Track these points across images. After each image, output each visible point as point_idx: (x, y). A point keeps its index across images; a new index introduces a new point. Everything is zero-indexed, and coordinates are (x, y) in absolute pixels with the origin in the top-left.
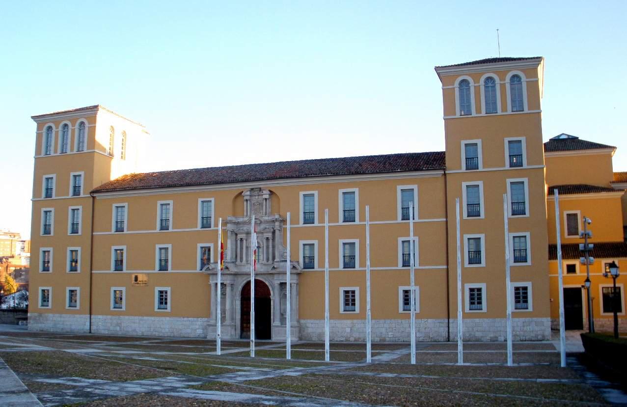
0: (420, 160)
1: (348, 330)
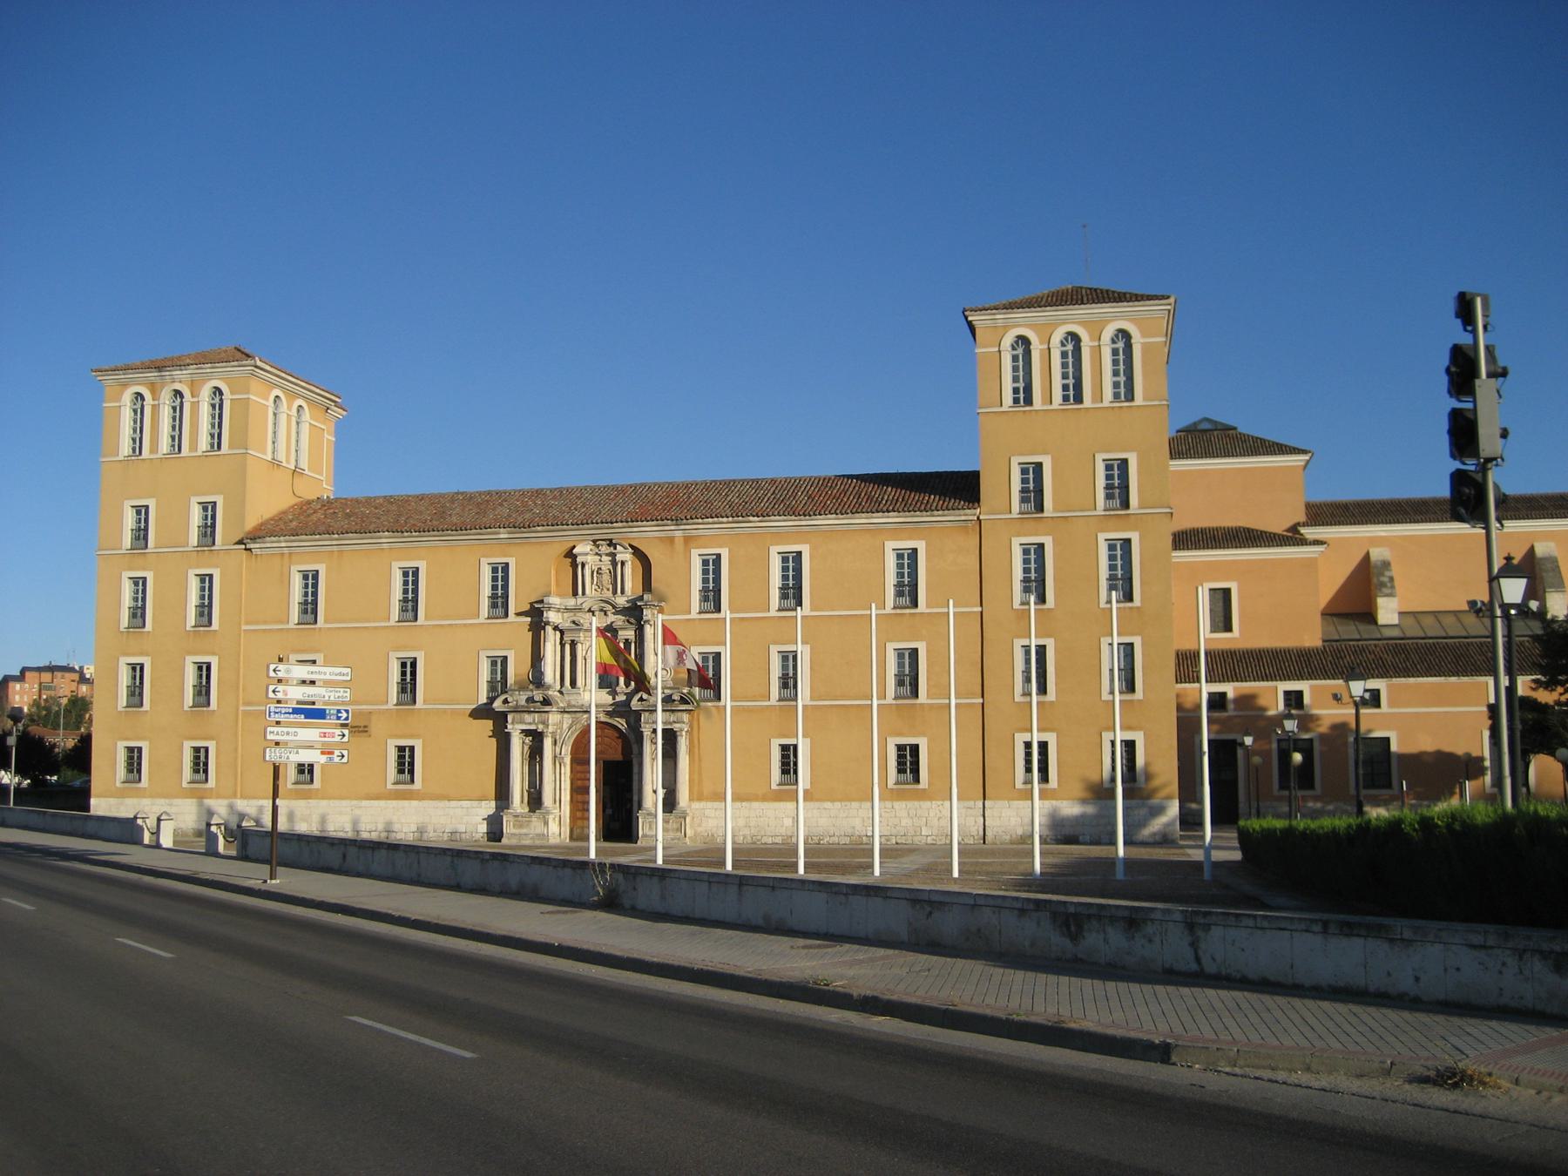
0: (736, 501)
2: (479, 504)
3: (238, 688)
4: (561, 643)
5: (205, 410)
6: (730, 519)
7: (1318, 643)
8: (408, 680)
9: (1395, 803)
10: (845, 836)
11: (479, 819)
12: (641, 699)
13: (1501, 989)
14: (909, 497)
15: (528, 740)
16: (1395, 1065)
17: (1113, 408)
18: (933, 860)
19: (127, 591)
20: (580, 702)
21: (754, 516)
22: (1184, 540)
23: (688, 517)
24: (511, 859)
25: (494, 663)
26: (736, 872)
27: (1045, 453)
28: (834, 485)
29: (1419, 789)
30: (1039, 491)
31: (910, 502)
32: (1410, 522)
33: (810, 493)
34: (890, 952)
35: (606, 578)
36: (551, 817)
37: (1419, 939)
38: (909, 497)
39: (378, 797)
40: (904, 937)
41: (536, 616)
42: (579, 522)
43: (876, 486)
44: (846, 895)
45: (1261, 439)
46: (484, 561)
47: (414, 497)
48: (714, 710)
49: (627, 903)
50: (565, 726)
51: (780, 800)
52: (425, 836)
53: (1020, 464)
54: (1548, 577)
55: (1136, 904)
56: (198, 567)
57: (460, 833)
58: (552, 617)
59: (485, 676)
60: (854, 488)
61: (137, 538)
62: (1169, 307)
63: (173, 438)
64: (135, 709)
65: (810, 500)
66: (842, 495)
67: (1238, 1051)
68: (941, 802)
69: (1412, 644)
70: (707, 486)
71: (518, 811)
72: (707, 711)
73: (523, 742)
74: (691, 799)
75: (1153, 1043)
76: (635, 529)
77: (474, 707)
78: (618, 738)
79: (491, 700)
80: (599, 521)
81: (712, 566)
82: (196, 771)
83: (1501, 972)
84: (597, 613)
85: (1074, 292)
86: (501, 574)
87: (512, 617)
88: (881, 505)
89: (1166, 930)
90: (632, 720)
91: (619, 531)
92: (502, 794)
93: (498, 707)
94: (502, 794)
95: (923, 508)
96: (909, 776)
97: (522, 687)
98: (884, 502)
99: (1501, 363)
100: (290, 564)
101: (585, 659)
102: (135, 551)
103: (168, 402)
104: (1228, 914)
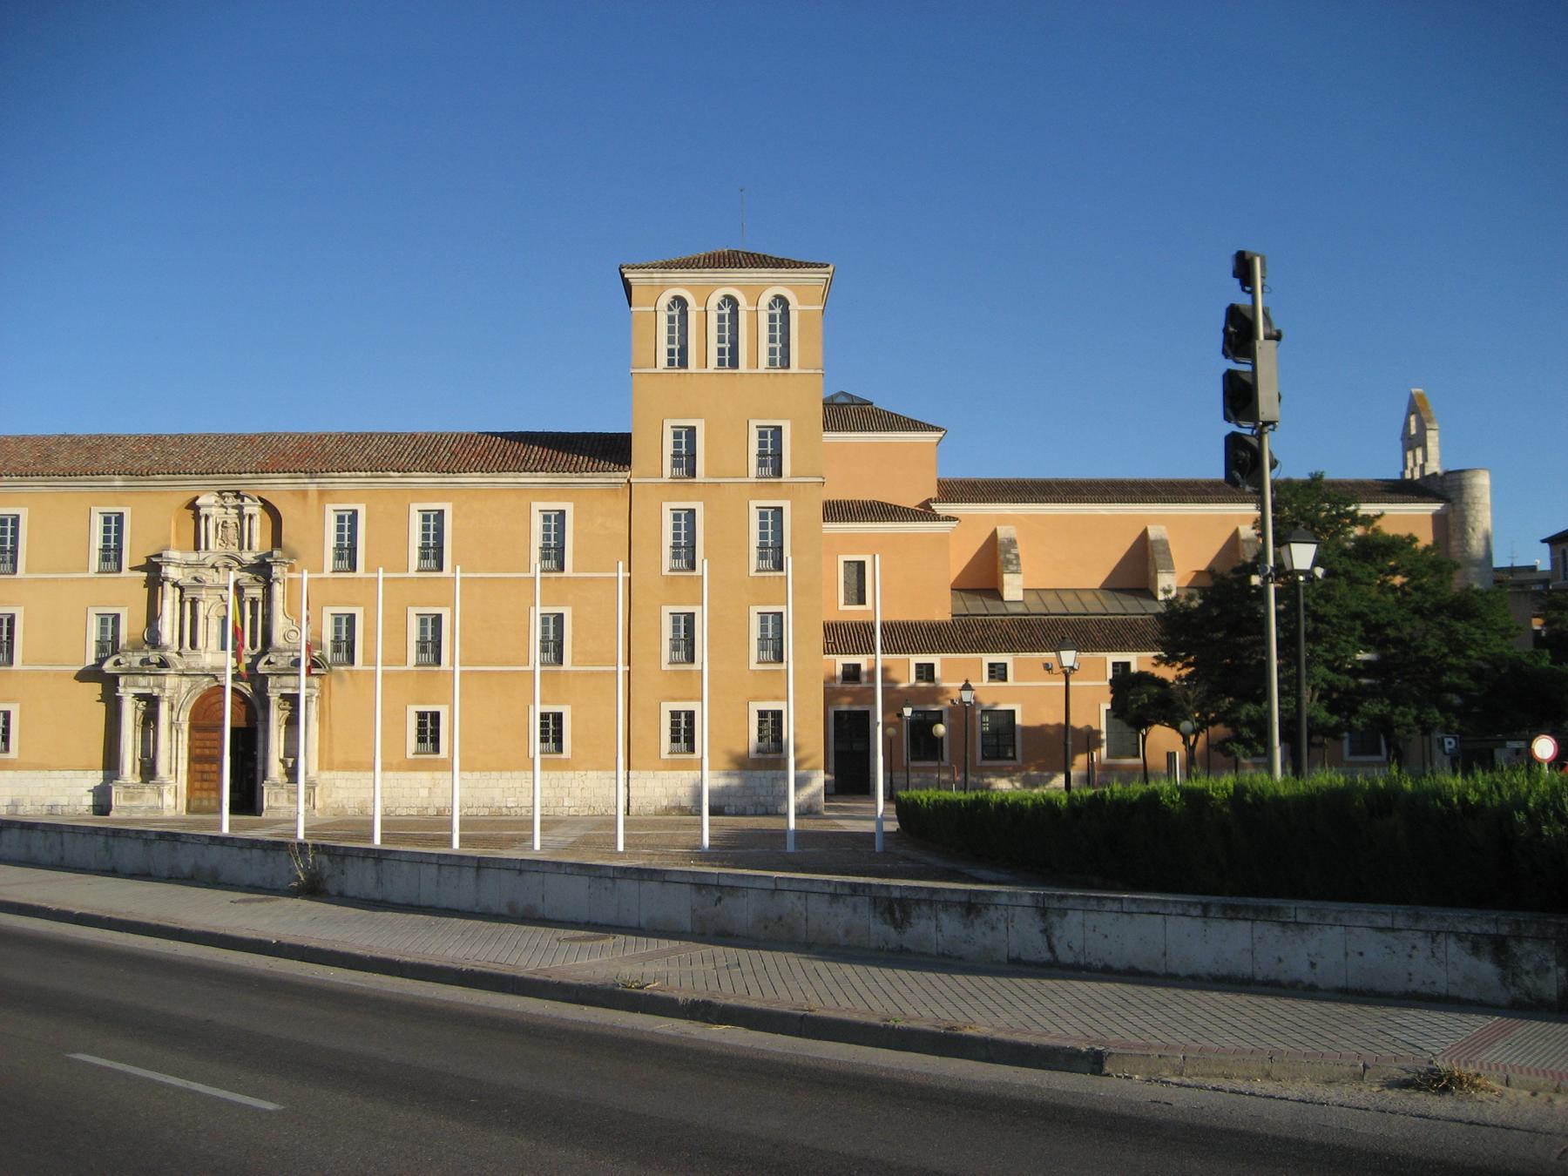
0: (374, 455)
1: (424, 793)
2: (89, 449)
4: (180, 601)
6: (369, 473)
7: (948, 618)
9: (1018, 774)
10: (483, 807)
11: (85, 790)
12: (269, 662)
13: (1410, 974)
14: (557, 456)
15: (142, 705)
16: (1369, 1068)
17: (768, 374)
18: (583, 833)
21: (394, 471)
22: (836, 511)
23: (324, 470)
24: (183, 840)
25: (104, 621)
26: (234, 835)
27: (698, 417)
28: (477, 442)
29: (1041, 761)
30: (692, 456)
31: (558, 462)
32: (1036, 502)
33: (453, 449)
34: (676, 944)
35: (232, 532)
36: (166, 788)
37: (1316, 922)
38: (557, 456)
40: (687, 925)
41: (153, 571)
42: (204, 471)
43: (522, 445)
44: (614, 879)
45: (896, 415)
46: (96, 511)
47: (13, 437)
48: (346, 674)
49: (332, 887)
50: (184, 690)
51: (416, 770)
52: (21, 811)
53: (672, 427)
54: (1159, 559)
55: (862, 880)
57: (62, 806)
58: (171, 572)
59: (94, 634)
60: (499, 446)
62: (827, 276)
65: (454, 457)
66: (487, 453)
67: (1184, 1058)
68: (585, 772)
69: (1036, 619)
70: (343, 438)
71: (129, 782)
72: (340, 675)
73: (136, 707)
74: (321, 768)
75: (1079, 1051)
76: (265, 481)
77: (81, 668)
78: (241, 703)
79: (101, 661)
80: (226, 471)
81: (348, 523)
83: (1410, 956)
84: (221, 570)
85: (731, 256)
86: (113, 525)
87: (125, 571)
88: (529, 464)
89: (1013, 915)
90: (258, 685)
91: (247, 482)
92: (111, 763)
94: (111, 763)
95: (572, 468)
96: (429, 745)
97: (136, 648)
98: (531, 461)
99: (1276, 326)
101: (207, 618)
104: (1090, 898)
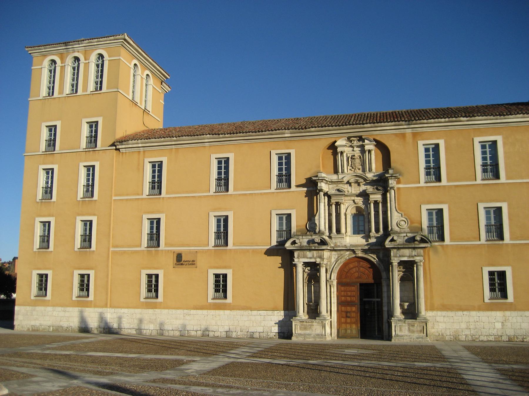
1: (499, 325)
3: (109, 236)
5: (93, 68)
8: (222, 230)
11: (273, 323)
19: (42, 177)
20: (344, 244)
35: (358, 161)
39: (202, 308)
48: (439, 247)
50: (333, 260)
51: (492, 310)
53: (480, 142)
56: (86, 161)
57: (259, 333)
61: (49, 145)
63: (73, 86)
64: (44, 250)
72: (435, 248)
74: (426, 310)
77: (268, 247)
78: (369, 268)
82: (82, 290)
84: (353, 184)
87: (293, 188)
93: (288, 247)
97: (304, 234)
100: (144, 157)
102: (47, 153)
103: (70, 65)
